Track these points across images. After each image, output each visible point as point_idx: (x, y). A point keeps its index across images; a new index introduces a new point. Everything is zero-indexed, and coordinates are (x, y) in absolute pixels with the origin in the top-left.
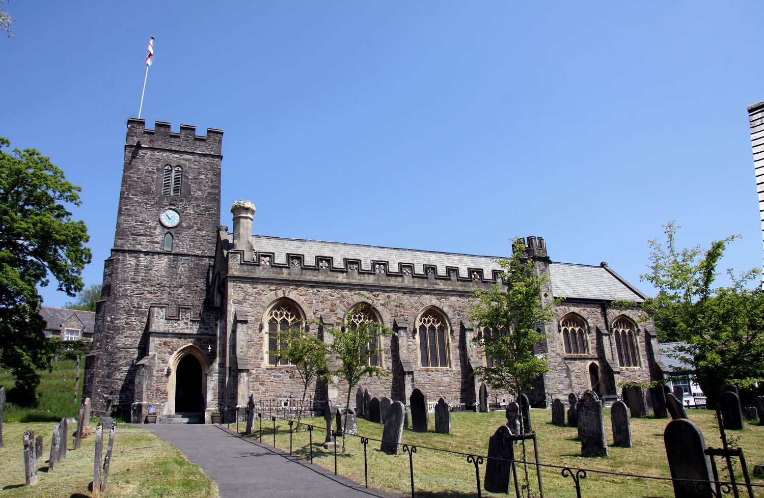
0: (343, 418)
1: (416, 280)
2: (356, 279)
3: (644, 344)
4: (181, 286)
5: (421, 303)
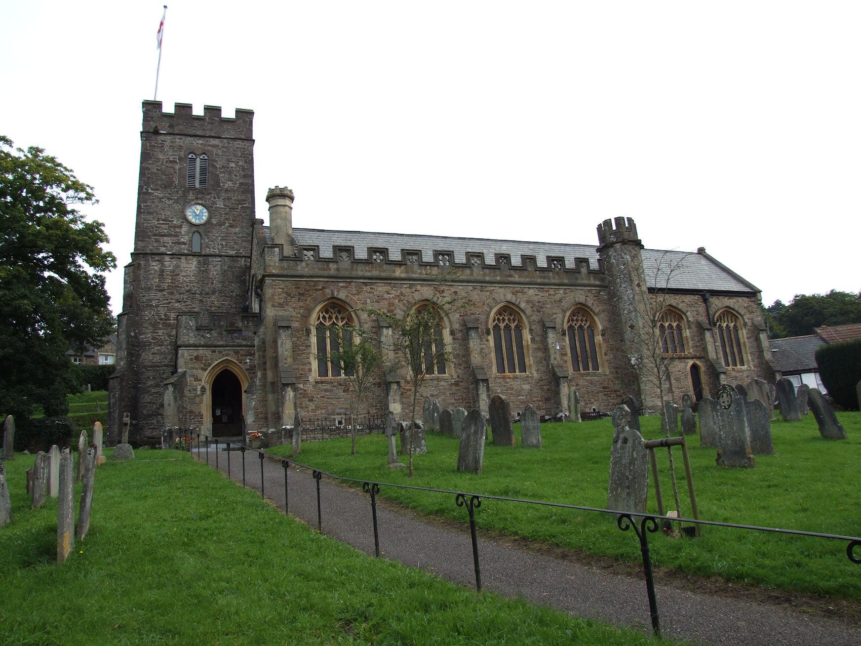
0: (407, 434)
1: (487, 271)
2: (418, 272)
3: (752, 340)
4: (214, 292)
5: (494, 299)
